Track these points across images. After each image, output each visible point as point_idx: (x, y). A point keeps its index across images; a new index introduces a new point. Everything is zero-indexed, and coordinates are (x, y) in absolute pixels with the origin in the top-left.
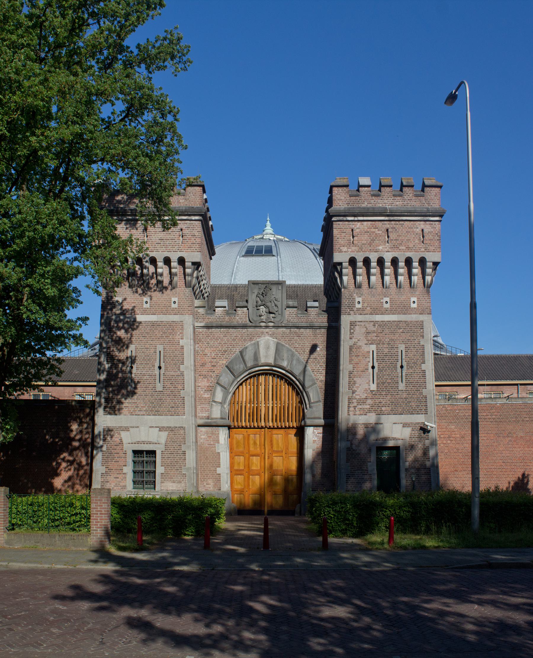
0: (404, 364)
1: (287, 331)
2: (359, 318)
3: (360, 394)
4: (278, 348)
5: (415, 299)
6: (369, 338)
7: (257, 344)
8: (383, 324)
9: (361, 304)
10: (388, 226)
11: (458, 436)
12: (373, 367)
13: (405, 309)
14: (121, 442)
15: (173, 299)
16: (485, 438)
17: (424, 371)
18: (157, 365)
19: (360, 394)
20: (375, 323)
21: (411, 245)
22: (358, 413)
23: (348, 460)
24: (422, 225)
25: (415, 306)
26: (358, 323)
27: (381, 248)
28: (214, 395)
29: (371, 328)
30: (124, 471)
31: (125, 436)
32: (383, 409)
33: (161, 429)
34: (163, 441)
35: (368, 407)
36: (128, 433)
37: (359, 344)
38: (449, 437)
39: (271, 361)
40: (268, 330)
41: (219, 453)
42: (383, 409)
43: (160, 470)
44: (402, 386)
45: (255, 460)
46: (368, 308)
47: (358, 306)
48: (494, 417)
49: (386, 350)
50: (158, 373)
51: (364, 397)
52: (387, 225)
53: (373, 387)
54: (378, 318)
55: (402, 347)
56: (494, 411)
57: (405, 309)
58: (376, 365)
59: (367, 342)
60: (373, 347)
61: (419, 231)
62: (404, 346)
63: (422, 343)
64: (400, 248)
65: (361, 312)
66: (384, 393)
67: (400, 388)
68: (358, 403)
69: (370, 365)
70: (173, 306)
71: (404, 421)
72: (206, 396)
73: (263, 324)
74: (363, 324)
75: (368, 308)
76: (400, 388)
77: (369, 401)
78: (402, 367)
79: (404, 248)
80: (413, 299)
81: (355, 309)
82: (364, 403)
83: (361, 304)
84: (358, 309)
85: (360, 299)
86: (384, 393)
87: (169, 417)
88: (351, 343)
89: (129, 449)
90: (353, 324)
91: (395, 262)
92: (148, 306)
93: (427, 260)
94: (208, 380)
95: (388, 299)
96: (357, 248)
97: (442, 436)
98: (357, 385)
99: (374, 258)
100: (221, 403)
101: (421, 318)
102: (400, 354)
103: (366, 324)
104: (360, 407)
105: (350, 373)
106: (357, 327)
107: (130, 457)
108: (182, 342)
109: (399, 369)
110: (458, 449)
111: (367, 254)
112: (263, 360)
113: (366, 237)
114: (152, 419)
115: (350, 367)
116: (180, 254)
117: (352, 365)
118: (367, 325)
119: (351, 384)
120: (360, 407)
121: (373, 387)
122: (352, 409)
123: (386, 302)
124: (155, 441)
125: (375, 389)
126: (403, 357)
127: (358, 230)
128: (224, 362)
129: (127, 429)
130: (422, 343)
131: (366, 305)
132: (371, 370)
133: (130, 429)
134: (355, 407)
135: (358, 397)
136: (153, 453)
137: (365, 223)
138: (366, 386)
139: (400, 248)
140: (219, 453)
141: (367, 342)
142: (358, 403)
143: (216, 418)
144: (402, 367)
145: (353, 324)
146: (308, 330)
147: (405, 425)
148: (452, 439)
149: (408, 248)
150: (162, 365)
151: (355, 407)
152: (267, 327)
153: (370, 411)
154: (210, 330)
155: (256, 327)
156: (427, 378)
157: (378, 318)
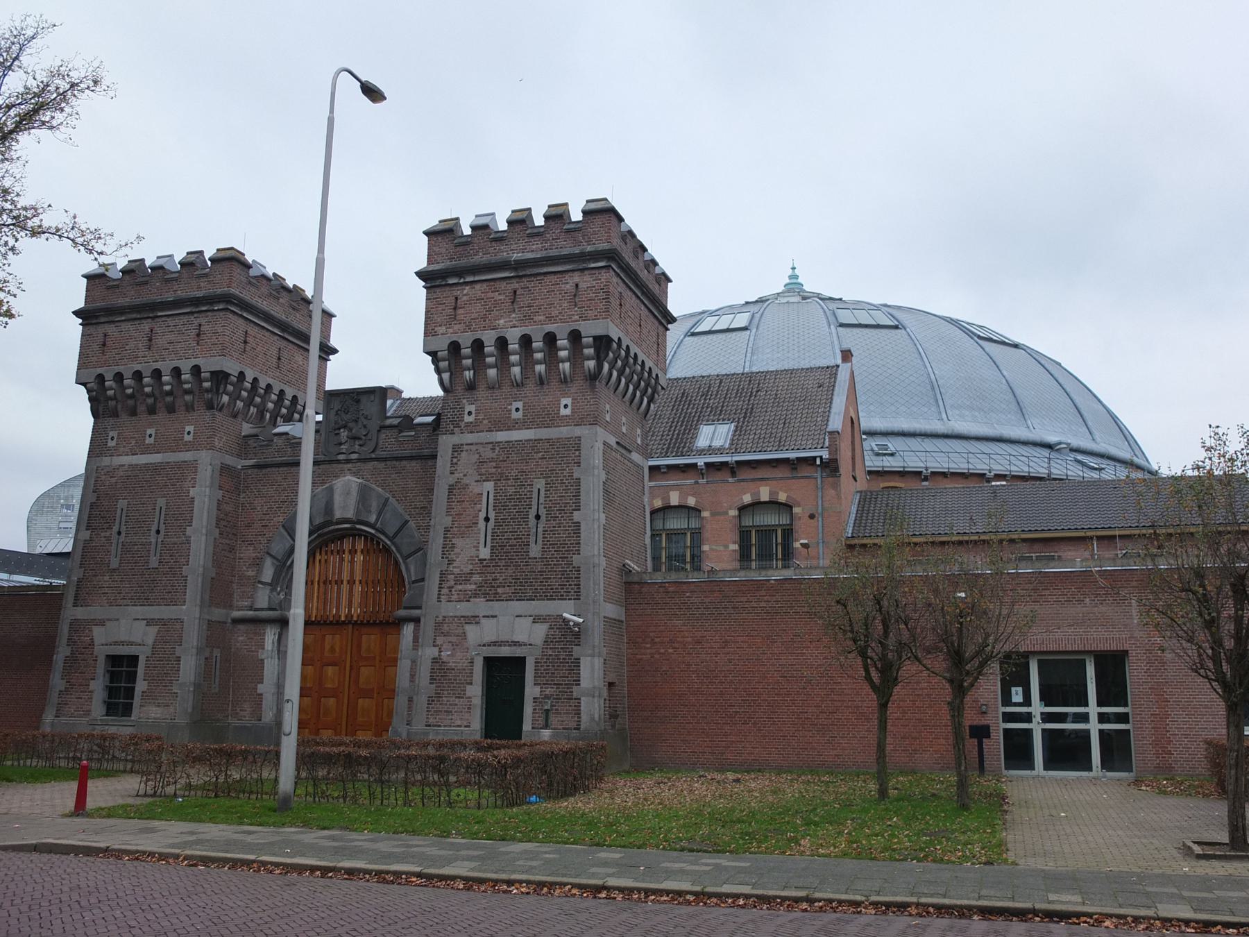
0: (543, 512)
1: (381, 465)
2: (469, 438)
3: (462, 564)
4: (364, 493)
5: (568, 401)
6: (483, 471)
7: (331, 490)
8: (509, 446)
9: (521, 412)
10: (517, 286)
11: (690, 639)
12: (487, 519)
13: (551, 419)
14: (92, 644)
15: (188, 429)
16: (745, 645)
17: (578, 524)
18: (154, 528)
19: (462, 564)
20: (494, 445)
21: (555, 313)
22: (455, 597)
23: (432, 679)
24: (576, 278)
25: (568, 412)
26: (465, 447)
27: (502, 321)
28: (260, 571)
29: (488, 453)
30: (91, 688)
31: (98, 633)
32: (499, 590)
33: (150, 622)
34: (150, 641)
35: (474, 587)
36: (102, 629)
37: (466, 481)
38: (671, 641)
39: (350, 514)
40: (350, 466)
41: (262, 660)
42: (499, 590)
43: (141, 686)
44: (535, 550)
45: (330, 671)
46: (485, 422)
47: (468, 419)
48: (763, 604)
49: (511, 490)
50: (153, 540)
51: (467, 570)
52: (515, 285)
53: (485, 553)
54: (502, 436)
55: (540, 484)
56: (763, 593)
57: (551, 419)
58: (492, 515)
59: (478, 478)
60: (489, 486)
61: (569, 287)
62: (543, 481)
63: (576, 475)
64: (536, 318)
65: (473, 428)
66: (502, 563)
67: (532, 555)
68: (457, 581)
69: (482, 515)
70: (187, 438)
71: (537, 612)
72: (250, 573)
73: (341, 457)
74: (474, 448)
75: (485, 422)
76: (532, 555)
77: (476, 578)
78: (538, 517)
79: (542, 318)
80: (564, 401)
81: (463, 425)
82: (467, 580)
83: (521, 412)
84: (468, 424)
85: (473, 408)
86: (502, 563)
87: (163, 608)
88: (452, 480)
89: (101, 652)
90: (457, 449)
91: (526, 341)
92: (152, 440)
93: (583, 334)
94: (255, 548)
95: (520, 405)
96: (462, 327)
97: (657, 640)
98: (456, 551)
99: (489, 338)
100: (270, 584)
101: (578, 431)
102: (535, 495)
103: (481, 449)
104: (460, 587)
105: (447, 530)
106: (464, 454)
107: (101, 667)
108: (192, 492)
109: (532, 521)
110: (689, 665)
111: (478, 335)
112: (338, 514)
113: (479, 307)
114: (138, 611)
115: (448, 521)
116: (194, 362)
117: (450, 518)
118: (481, 449)
119: (448, 547)
120: (460, 587)
121: (485, 553)
122: (445, 591)
123: (517, 409)
124: (139, 641)
125: (488, 557)
126: (491, 501)
127: (465, 298)
128: (281, 519)
129: (101, 623)
130: (576, 475)
131: (481, 416)
132: (482, 524)
133: (483, 621)
134: (450, 588)
135: (456, 571)
136: (134, 660)
137: (478, 286)
138: (473, 552)
139: (536, 318)
140: (262, 660)
141: (478, 478)
142: (457, 581)
143: (262, 609)
144: (538, 517)
145: (457, 449)
146: (414, 463)
147: (537, 619)
148: (676, 645)
149: (550, 318)
150: (162, 527)
151: (450, 588)
152: (348, 461)
153: (476, 595)
154: (264, 471)
155: (330, 462)
156: (583, 535)
157: (502, 436)
